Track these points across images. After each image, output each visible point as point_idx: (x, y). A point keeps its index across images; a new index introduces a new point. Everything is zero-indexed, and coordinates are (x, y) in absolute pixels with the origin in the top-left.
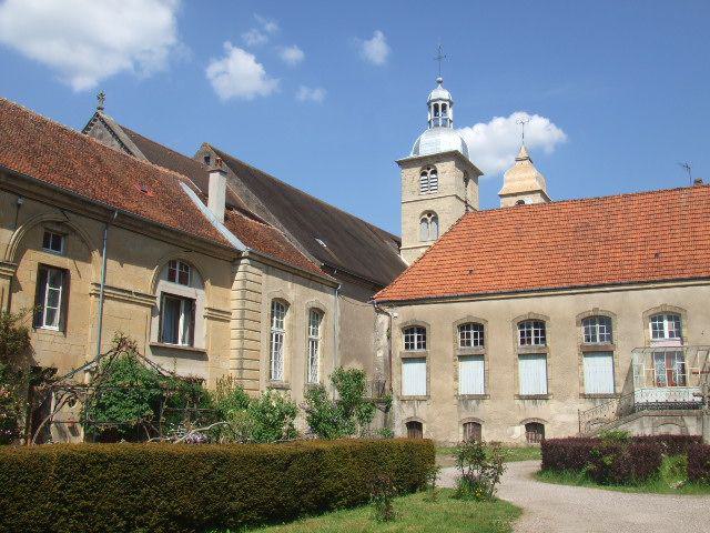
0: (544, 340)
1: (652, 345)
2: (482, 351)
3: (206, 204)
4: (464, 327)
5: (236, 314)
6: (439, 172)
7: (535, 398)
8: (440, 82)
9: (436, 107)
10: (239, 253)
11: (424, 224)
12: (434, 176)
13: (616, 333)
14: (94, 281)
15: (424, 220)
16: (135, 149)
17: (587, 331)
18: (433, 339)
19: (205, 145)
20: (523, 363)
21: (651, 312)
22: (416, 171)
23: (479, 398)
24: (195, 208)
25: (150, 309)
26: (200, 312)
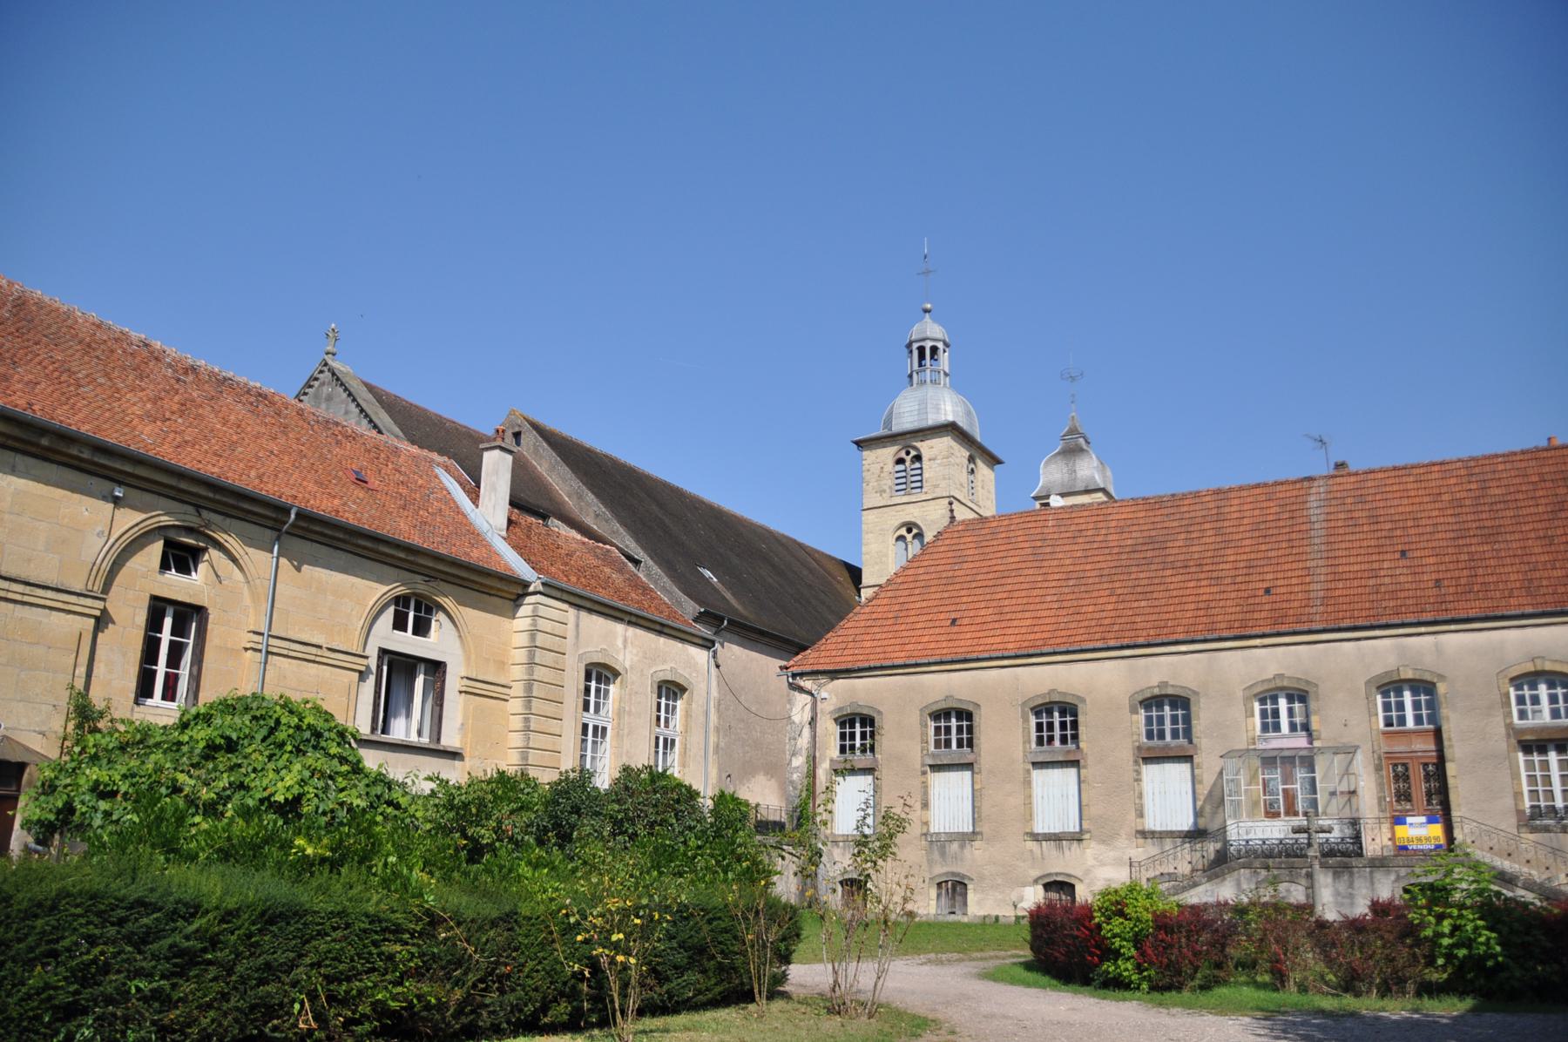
0: (1075, 737)
1: (1260, 746)
2: (969, 758)
3: (474, 495)
4: (1043, 709)
5: (518, 689)
6: (924, 459)
7: (1056, 838)
8: (926, 311)
9: (921, 350)
10: (526, 585)
11: (901, 543)
12: (917, 465)
13: (1198, 726)
14: (252, 628)
15: (901, 538)
16: (383, 418)
17: (1149, 720)
18: (887, 742)
19: (512, 413)
20: (1038, 776)
21: (1259, 689)
22: (888, 453)
23: (966, 839)
24: (458, 511)
25: (357, 674)
26: (453, 683)
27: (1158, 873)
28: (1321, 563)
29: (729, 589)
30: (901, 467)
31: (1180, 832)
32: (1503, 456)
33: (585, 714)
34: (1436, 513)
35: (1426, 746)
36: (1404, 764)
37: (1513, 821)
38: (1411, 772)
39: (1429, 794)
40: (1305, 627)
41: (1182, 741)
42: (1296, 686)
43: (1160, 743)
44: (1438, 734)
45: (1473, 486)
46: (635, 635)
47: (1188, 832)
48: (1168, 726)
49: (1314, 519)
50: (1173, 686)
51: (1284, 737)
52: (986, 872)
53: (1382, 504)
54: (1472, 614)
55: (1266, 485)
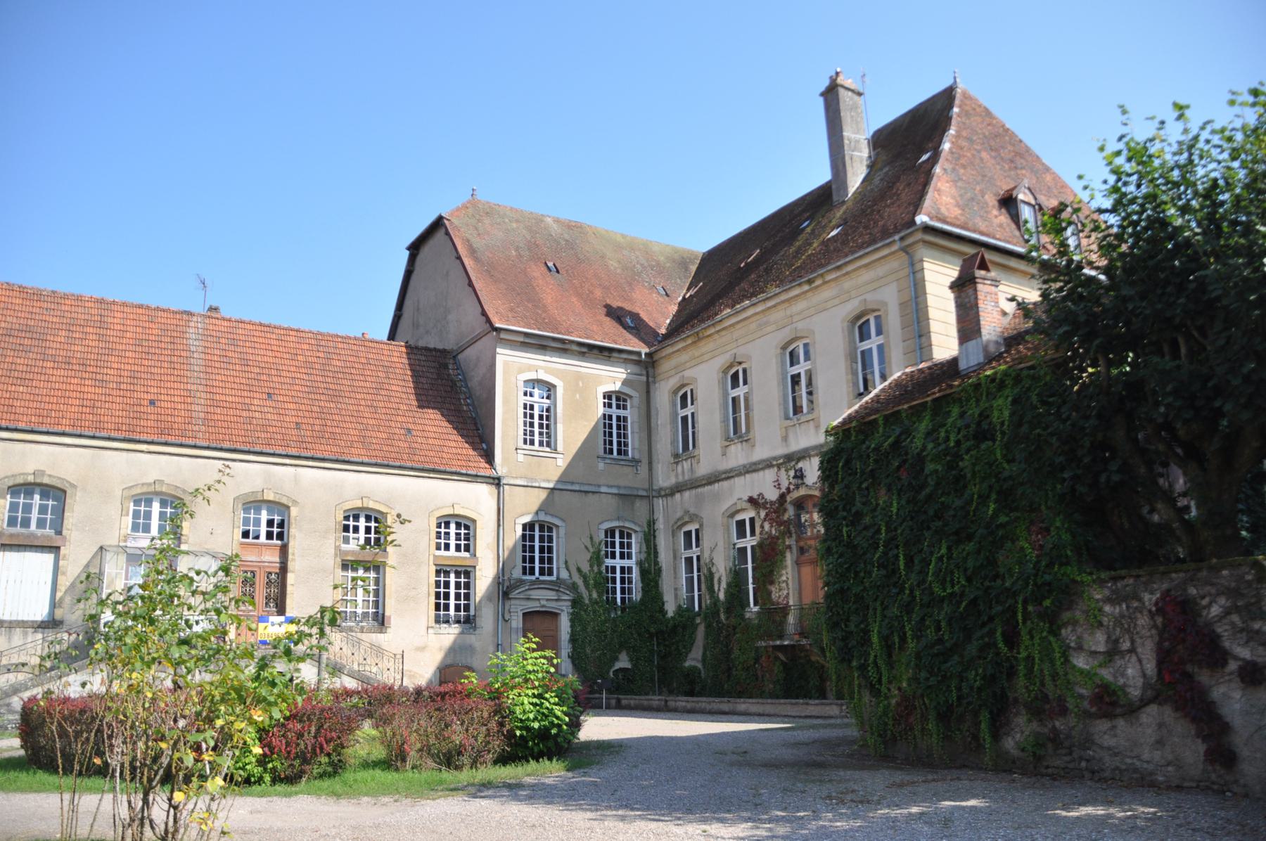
13: (70, 519)
17: (14, 507)
28: (201, 388)
31: (33, 622)
32: (342, 337)
34: (293, 369)
35: (272, 558)
36: (252, 572)
38: (257, 580)
39: (268, 598)
40: (191, 442)
41: (48, 531)
42: (173, 493)
43: (23, 530)
44: (284, 550)
45: (321, 355)
47: (42, 622)
48: (34, 515)
49: (193, 349)
50: (50, 476)
53: (250, 351)
54: (326, 455)
55: (148, 308)
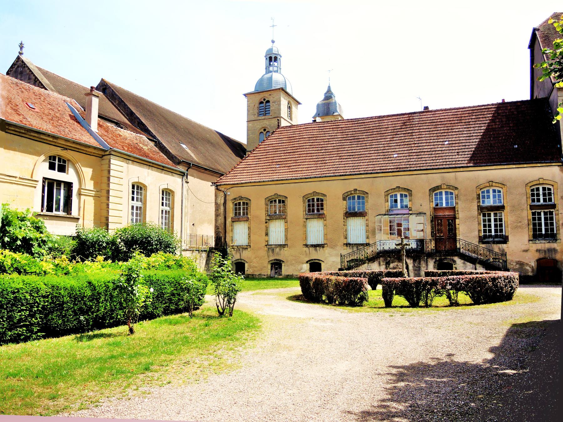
24: (495, 211)
27: (351, 259)
29: (193, 152)
30: (262, 105)
33: (133, 202)
37: (478, 240)
46: (148, 173)
51: (399, 209)
52: (289, 259)
